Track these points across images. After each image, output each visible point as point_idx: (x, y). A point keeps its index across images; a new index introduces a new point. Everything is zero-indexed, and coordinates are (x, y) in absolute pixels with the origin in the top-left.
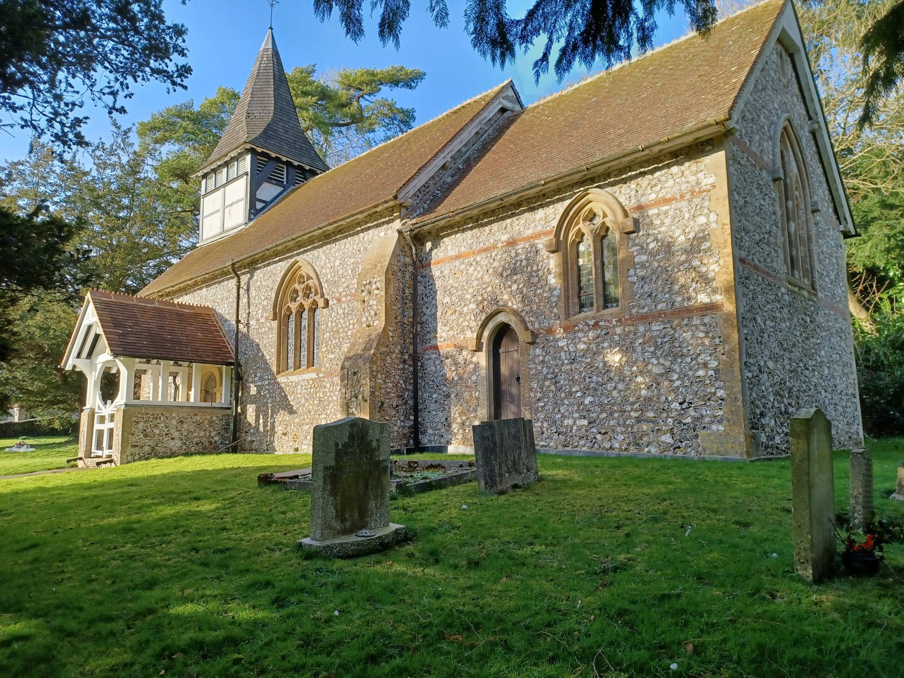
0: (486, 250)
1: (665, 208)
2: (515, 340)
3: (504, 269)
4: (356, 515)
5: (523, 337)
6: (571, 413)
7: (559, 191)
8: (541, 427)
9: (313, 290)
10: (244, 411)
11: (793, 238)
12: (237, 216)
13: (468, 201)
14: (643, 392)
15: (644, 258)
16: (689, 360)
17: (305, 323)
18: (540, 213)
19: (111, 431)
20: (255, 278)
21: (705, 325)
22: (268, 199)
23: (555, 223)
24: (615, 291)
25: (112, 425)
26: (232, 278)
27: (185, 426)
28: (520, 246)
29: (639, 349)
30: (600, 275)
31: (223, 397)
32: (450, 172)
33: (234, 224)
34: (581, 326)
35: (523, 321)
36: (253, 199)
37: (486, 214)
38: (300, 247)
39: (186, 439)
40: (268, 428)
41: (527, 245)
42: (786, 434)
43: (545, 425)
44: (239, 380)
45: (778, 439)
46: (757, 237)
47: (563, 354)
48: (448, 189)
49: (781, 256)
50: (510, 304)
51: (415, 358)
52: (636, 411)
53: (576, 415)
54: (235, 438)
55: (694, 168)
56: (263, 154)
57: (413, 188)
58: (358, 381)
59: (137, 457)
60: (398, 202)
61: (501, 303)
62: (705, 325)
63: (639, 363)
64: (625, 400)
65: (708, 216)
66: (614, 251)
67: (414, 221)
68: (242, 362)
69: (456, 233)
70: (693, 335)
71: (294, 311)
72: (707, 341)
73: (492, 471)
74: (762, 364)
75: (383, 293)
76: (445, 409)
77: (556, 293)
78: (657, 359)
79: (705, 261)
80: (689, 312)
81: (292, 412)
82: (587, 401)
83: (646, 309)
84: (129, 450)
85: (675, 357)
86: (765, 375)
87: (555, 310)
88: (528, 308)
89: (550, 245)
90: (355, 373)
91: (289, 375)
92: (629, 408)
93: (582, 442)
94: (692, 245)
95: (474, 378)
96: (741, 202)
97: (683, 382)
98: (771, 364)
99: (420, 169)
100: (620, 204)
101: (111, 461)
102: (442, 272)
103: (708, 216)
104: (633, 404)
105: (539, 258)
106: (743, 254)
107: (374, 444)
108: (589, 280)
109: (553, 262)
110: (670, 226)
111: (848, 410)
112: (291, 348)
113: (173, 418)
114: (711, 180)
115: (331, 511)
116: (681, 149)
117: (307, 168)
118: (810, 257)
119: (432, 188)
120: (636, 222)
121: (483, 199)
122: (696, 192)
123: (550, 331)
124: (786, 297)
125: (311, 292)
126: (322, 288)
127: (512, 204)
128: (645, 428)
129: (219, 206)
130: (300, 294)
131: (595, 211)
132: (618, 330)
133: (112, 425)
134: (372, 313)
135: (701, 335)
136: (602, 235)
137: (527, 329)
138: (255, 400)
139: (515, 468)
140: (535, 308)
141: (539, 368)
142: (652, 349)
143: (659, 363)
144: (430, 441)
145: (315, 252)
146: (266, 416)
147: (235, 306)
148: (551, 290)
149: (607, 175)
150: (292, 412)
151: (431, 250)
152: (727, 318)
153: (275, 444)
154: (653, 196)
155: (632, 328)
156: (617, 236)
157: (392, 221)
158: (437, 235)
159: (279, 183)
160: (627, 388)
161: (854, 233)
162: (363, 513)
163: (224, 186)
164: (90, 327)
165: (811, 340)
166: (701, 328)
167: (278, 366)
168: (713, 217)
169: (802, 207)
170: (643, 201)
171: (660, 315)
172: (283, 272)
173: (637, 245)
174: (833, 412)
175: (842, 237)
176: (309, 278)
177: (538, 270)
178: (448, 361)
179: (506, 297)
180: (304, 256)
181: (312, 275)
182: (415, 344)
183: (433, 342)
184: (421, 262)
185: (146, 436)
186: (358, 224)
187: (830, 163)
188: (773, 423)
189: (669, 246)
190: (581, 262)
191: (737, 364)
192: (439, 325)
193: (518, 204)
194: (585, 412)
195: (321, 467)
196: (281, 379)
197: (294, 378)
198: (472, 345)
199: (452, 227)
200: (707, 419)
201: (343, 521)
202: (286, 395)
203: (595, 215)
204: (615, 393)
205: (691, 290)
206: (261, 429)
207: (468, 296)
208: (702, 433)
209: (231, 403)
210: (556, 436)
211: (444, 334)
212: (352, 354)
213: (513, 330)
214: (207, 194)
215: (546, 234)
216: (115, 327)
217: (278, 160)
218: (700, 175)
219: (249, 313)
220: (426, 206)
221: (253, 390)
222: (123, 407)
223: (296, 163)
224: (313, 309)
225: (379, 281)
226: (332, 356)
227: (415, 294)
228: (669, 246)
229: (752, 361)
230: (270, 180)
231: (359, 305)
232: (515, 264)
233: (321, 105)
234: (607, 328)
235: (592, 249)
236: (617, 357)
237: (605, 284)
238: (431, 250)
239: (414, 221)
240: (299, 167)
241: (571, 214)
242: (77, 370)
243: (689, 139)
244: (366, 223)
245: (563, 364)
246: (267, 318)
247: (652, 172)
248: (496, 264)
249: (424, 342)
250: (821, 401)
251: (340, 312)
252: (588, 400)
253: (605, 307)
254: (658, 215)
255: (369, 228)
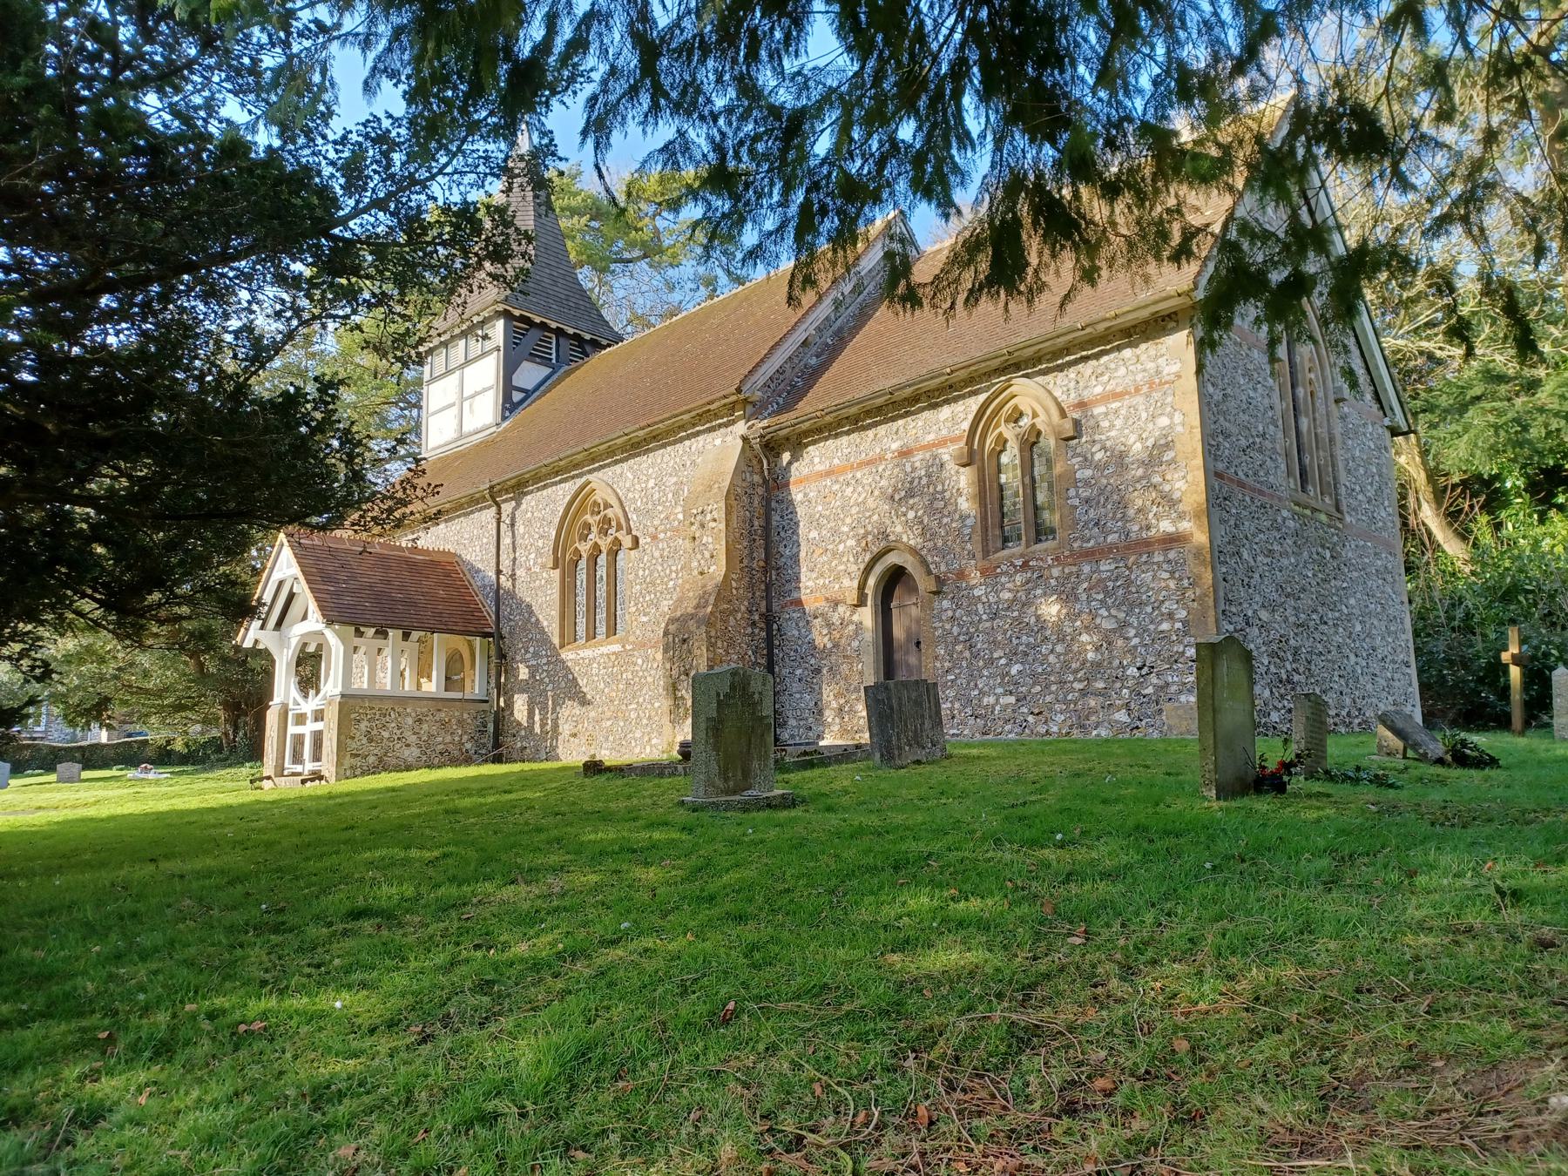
0: (869, 463)
1: (1115, 405)
2: (913, 589)
3: (896, 490)
4: (740, 775)
5: (924, 584)
6: (993, 688)
7: (971, 380)
8: (951, 709)
9: (614, 523)
10: (510, 705)
11: (1305, 439)
12: (484, 413)
13: (843, 395)
14: (1090, 656)
15: (1088, 473)
16: (1149, 609)
17: (602, 572)
18: (946, 412)
19: (318, 738)
20: (523, 506)
21: (1169, 562)
22: (530, 387)
23: (966, 425)
24: (1050, 518)
25: (319, 726)
26: (489, 507)
27: (425, 726)
28: (917, 458)
29: (1084, 597)
30: (1030, 497)
31: (476, 685)
32: (814, 350)
33: (479, 425)
34: (1004, 568)
35: (924, 562)
36: (508, 387)
37: (868, 413)
38: (593, 461)
39: (425, 746)
40: (548, 728)
41: (928, 455)
42: (1290, 711)
43: (957, 705)
44: (502, 660)
45: (1275, 717)
46: (1243, 443)
47: (980, 606)
48: (811, 375)
49: (1283, 467)
50: (905, 539)
51: (769, 619)
52: (1080, 681)
53: (1000, 690)
54: (497, 744)
55: (1152, 352)
56: (523, 319)
57: (762, 376)
58: (690, 652)
59: (358, 771)
60: (742, 396)
61: (892, 538)
62: (1169, 562)
63: (1084, 616)
64: (1066, 665)
65: (1171, 416)
66: (1049, 464)
67: (765, 423)
68: (505, 631)
69: (826, 439)
70: (1154, 577)
71: (585, 555)
72: (1172, 584)
73: (889, 742)
74: (1250, 613)
75: (722, 526)
76: (814, 690)
77: (969, 522)
78: (1108, 609)
79: (1168, 477)
80: (1145, 545)
81: (584, 702)
82: (1014, 671)
83: (1092, 543)
84: (348, 761)
85: (1132, 606)
86: (1256, 631)
87: (969, 546)
88: (930, 544)
89: (960, 456)
90: (684, 641)
91: (579, 648)
92: (1071, 678)
93: (1008, 727)
94: (1151, 455)
95: (855, 644)
96: (1218, 396)
97: (1142, 639)
98: (1264, 615)
99: (772, 348)
100: (1055, 399)
101: (321, 778)
102: (806, 495)
103: (1171, 416)
104: (1076, 671)
105: (945, 474)
106: (1221, 466)
107: (756, 696)
108: (1015, 504)
109: (963, 480)
110: (1122, 429)
111: (1397, 684)
112: (582, 609)
113: (408, 715)
114: (1175, 368)
115: (714, 767)
116: (1135, 326)
117: (588, 337)
118: (1333, 466)
119: (789, 371)
120: (1077, 424)
121: (864, 393)
122: (1156, 383)
123: (961, 575)
124: (1291, 524)
125: (610, 526)
126: (627, 520)
127: (905, 399)
128: (1093, 703)
129: (453, 397)
130: (594, 529)
131: (1021, 408)
132: (1056, 572)
133: (319, 726)
134: (707, 555)
135: (1166, 575)
136: (1030, 443)
137: (929, 572)
138: (525, 688)
139: (917, 742)
140: (940, 544)
141: (948, 626)
142: (1101, 596)
143: (1110, 615)
144: (792, 737)
145: (618, 468)
146: (544, 709)
147: (494, 551)
148: (963, 518)
149: (1036, 359)
150: (584, 702)
151: (790, 463)
152: (1198, 554)
153: (560, 751)
154: (1099, 389)
155: (1074, 569)
156: (1052, 442)
157: (733, 422)
158: (798, 442)
159: (545, 361)
160: (1068, 650)
161: (1405, 429)
162: (746, 773)
163: (462, 367)
164: (281, 583)
165: (1333, 582)
166: (1165, 566)
167: (562, 636)
168: (1178, 418)
169: (1321, 394)
170: (1086, 395)
171: (1110, 550)
172: (568, 498)
173: (1079, 455)
174: (1369, 686)
175: (1388, 434)
176: (607, 506)
177: (944, 491)
178: (817, 622)
179: (899, 529)
180: (600, 474)
181: (613, 501)
182: (768, 598)
183: (795, 595)
184: (775, 480)
185: (370, 740)
186: (682, 428)
187: (1364, 329)
188: (1267, 693)
189: (1122, 456)
190: (1003, 478)
191: (1212, 613)
192: (803, 570)
193: (915, 399)
194: (1011, 685)
195: (703, 718)
196: (567, 655)
197: (587, 653)
198: (852, 597)
199: (819, 430)
200: (1174, 688)
201: (726, 780)
202: (574, 679)
203: (1021, 414)
204: (1052, 658)
205: (1151, 515)
206: (537, 729)
207: (845, 529)
208: (1167, 706)
209: (488, 694)
210: (971, 721)
211: (810, 584)
212: (678, 614)
213: (910, 576)
214: (433, 379)
215: (954, 440)
216: (324, 582)
217: (543, 326)
218: (1161, 361)
219: (515, 559)
220: (781, 401)
221: (523, 673)
222: (338, 699)
223: (571, 331)
224: (613, 554)
225: (717, 509)
226: (645, 619)
227: (767, 528)
228: (1122, 456)
229: (1234, 610)
230: (532, 357)
231: (688, 544)
232: (911, 483)
233: (593, 229)
234: (1041, 568)
235: (1017, 462)
236: (1055, 609)
237: (1037, 509)
238: (790, 463)
239: (765, 423)
240: (576, 337)
241: (988, 412)
242: (261, 647)
243: (1145, 314)
244: (694, 425)
245: (980, 621)
246: (543, 566)
247: (1097, 356)
248: (884, 483)
249: (781, 595)
250: (1349, 669)
251: (657, 554)
252: (1014, 670)
253: (1038, 541)
254: (1106, 414)
255: (698, 434)
